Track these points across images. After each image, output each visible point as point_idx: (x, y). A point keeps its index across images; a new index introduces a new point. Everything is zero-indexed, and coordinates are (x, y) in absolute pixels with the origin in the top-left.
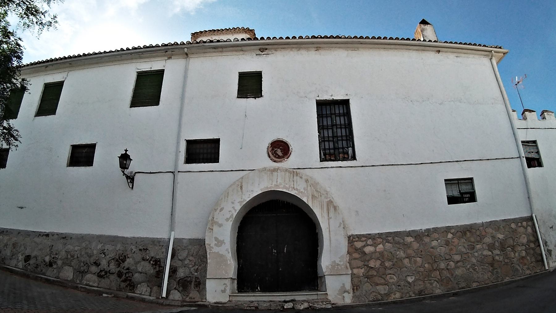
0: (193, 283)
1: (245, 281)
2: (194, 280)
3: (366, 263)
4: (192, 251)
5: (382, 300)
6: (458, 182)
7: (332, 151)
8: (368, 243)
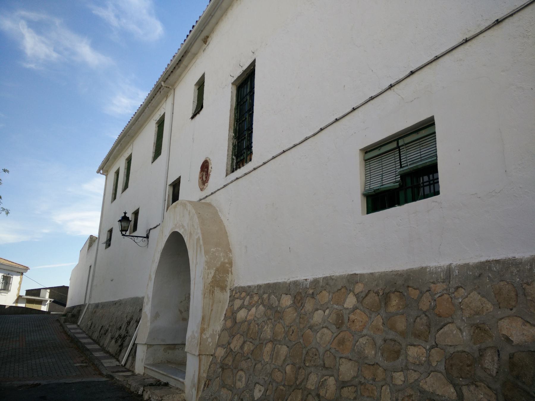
6: (395, 144)
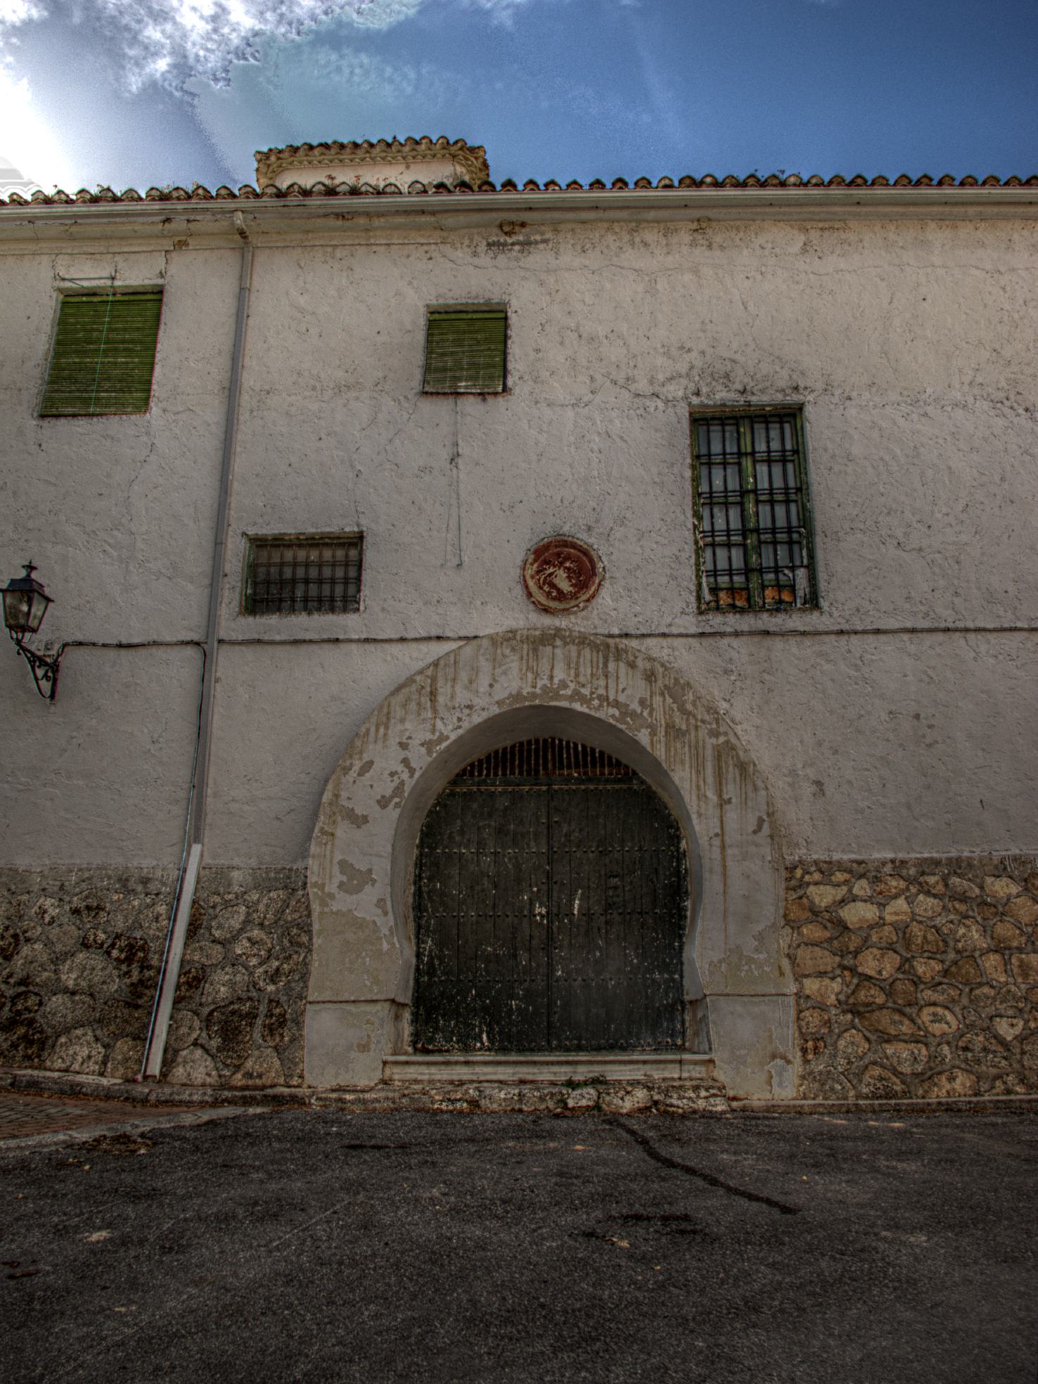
0: (259, 1021)
1: (440, 1008)
2: (263, 1009)
3: (848, 961)
4: (261, 907)
5: (905, 1094)
7: (739, 580)
8: (856, 891)
